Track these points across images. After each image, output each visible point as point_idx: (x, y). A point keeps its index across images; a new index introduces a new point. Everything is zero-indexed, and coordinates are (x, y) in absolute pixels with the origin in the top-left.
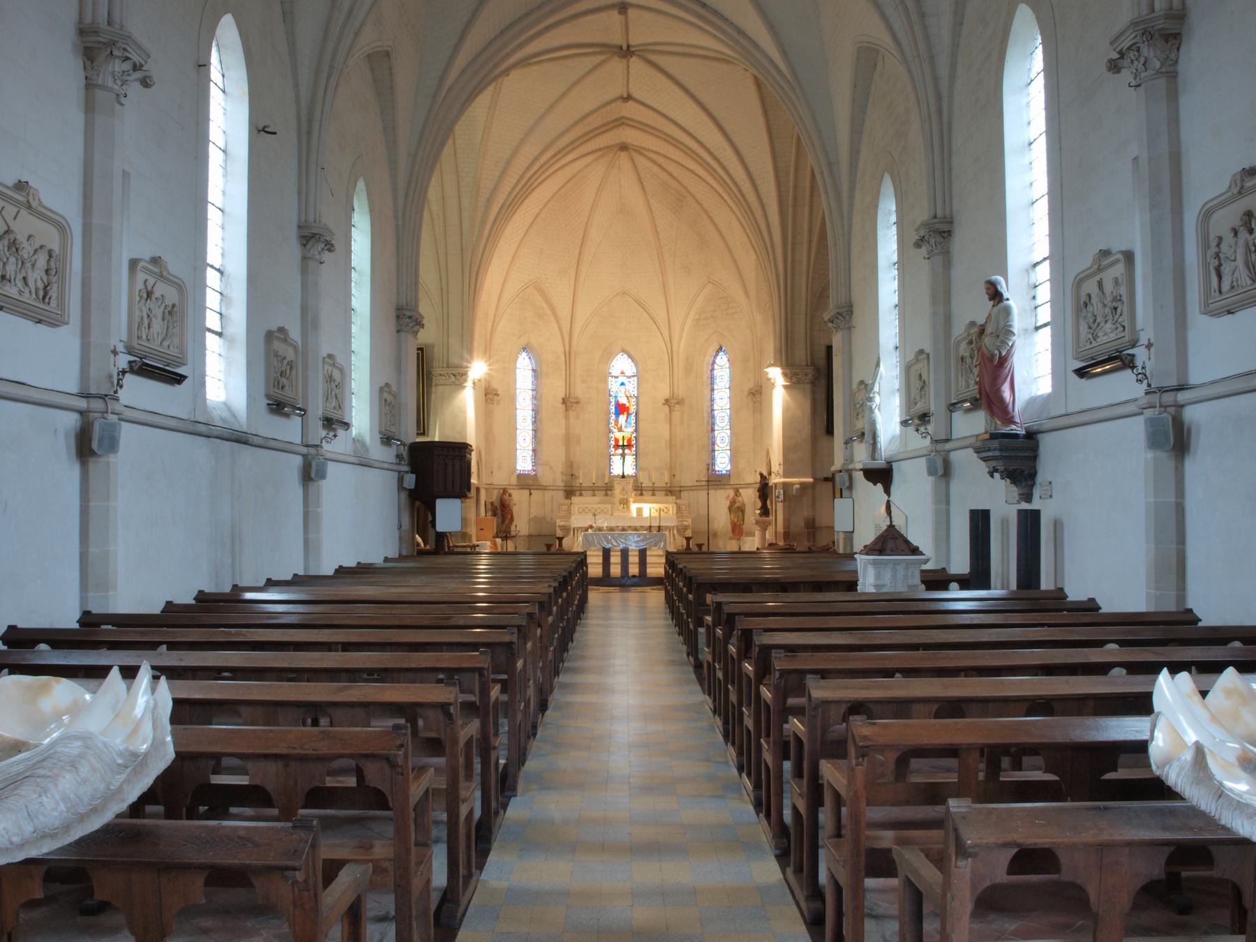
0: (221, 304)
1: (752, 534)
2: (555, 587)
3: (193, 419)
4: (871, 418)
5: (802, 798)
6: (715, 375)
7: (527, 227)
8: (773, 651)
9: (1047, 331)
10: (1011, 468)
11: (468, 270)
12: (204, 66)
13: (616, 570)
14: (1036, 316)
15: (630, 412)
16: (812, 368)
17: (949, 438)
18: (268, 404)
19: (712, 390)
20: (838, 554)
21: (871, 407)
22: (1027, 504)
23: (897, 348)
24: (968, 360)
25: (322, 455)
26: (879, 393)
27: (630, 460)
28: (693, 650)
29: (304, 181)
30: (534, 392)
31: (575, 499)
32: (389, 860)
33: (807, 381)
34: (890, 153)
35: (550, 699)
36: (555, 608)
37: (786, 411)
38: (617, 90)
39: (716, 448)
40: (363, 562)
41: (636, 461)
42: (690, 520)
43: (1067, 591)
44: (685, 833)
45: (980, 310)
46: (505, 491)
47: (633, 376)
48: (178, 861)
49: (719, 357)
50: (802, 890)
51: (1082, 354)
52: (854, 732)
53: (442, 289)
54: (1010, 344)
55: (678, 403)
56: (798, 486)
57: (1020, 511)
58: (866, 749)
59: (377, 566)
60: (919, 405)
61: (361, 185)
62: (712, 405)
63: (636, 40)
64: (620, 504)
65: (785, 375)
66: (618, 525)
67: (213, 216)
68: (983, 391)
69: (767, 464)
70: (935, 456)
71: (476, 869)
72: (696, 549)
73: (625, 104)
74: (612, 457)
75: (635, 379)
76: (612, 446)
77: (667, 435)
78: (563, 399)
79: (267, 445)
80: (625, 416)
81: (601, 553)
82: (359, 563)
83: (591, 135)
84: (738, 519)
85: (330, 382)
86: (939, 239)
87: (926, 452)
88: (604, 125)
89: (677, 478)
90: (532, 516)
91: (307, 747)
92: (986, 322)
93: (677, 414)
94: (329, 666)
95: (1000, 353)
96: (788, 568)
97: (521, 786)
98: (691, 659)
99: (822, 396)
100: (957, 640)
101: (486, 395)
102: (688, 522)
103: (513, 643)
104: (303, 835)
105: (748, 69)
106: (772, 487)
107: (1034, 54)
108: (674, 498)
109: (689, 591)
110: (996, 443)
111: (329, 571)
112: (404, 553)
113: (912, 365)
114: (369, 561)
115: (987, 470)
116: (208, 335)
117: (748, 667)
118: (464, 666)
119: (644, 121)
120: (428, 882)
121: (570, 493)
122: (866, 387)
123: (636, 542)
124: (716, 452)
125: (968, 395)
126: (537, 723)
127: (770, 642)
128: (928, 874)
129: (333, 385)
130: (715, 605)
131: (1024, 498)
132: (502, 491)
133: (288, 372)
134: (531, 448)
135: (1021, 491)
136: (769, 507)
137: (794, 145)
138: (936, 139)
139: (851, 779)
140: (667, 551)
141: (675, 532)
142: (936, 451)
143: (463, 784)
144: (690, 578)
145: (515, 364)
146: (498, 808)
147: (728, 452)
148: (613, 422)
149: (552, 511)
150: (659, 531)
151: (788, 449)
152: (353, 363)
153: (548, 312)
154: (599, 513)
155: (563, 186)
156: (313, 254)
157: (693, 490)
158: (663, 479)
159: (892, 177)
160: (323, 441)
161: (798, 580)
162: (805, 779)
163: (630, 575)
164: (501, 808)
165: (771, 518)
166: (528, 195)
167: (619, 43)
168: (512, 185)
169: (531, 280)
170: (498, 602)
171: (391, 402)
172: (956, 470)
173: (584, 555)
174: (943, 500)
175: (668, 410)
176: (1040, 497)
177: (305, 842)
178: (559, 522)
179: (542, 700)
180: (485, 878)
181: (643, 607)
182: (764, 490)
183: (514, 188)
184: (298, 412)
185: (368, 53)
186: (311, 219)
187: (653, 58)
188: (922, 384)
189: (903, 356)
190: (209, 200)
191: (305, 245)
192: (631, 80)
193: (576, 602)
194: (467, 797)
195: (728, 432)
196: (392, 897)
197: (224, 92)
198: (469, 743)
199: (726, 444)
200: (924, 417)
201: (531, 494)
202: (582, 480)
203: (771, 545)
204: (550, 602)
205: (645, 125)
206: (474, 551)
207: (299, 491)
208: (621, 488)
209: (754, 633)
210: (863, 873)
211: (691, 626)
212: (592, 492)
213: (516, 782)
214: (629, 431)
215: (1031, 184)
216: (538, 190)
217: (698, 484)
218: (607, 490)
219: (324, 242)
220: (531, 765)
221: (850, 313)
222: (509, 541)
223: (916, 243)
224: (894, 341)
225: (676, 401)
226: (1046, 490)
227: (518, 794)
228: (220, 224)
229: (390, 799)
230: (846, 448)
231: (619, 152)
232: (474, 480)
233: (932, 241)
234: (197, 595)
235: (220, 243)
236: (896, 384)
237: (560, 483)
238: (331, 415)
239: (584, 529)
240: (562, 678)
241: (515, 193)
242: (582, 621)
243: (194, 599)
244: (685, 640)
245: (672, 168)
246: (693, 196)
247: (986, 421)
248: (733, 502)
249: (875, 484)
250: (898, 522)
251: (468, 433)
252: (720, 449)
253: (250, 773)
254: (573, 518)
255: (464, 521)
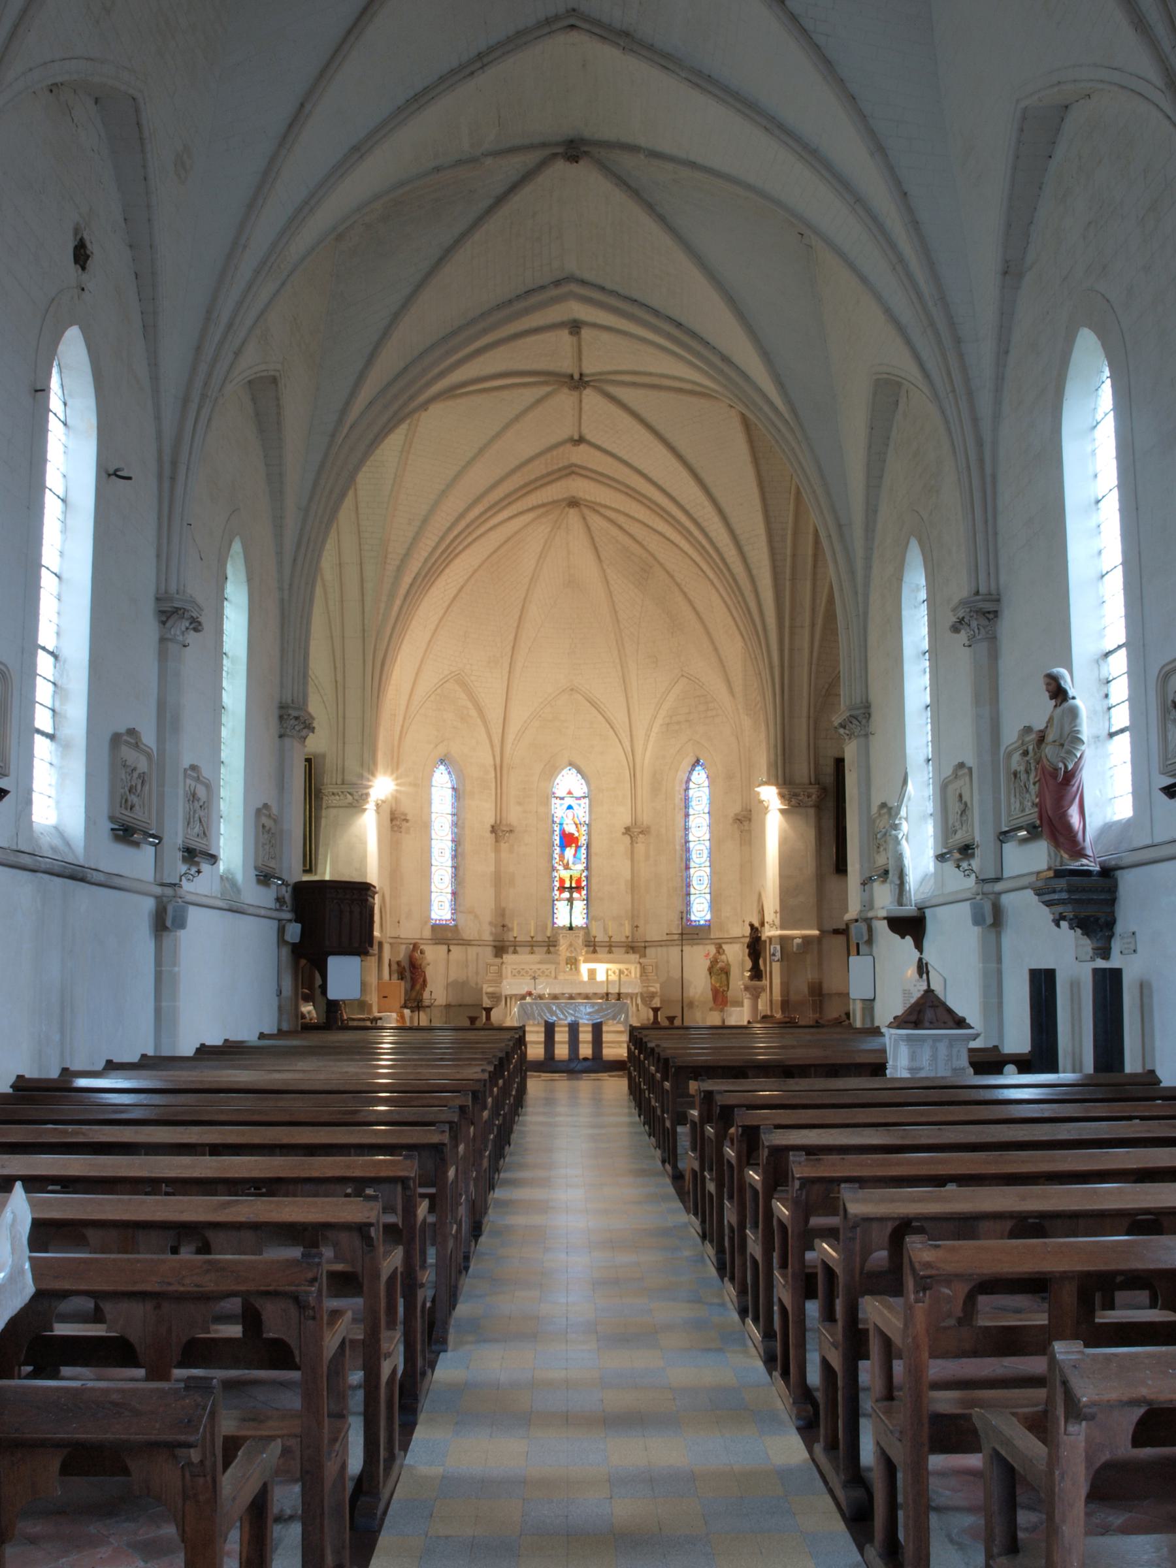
0: (53, 697)
1: (740, 1004)
2: (490, 1072)
3: (14, 847)
4: (897, 851)
5: (836, 1348)
6: (690, 796)
7: (446, 604)
8: (791, 1153)
9: (1125, 740)
10: (1082, 915)
11: (371, 657)
12: (41, 391)
13: (562, 1051)
14: (1109, 719)
15: (579, 844)
16: (817, 786)
17: (1000, 876)
18: (112, 829)
19: (687, 815)
20: (856, 1029)
21: (897, 837)
22: (1104, 961)
23: (929, 760)
24: (1023, 776)
25: (180, 898)
26: (906, 819)
27: (579, 906)
28: (670, 1155)
29: (165, 541)
30: (455, 818)
31: (508, 958)
32: (296, 1436)
33: (811, 803)
34: (917, 512)
35: (485, 1220)
36: (490, 1100)
37: (783, 842)
38: (567, 430)
39: (692, 891)
40: (232, 1039)
41: (587, 908)
42: (658, 986)
43: (1160, 1073)
44: (674, 1399)
45: (1039, 711)
46: (415, 946)
47: (584, 797)
48: (29, 1436)
49: (695, 773)
50: (838, 1474)
51: (1171, 768)
52: (913, 1257)
53: (336, 682)
54: (1078, 756)
55: (642, 832)
56: (799, 941)
57: (1096, 971)
58: (928, 1280)
59: (251, 1044)
60: (959, 835)
61: (237, 547)
62: (687, 835)
63: (589, 368)
64: (567, 964)
65: (782, 796)
66: (564, 992)
67: (48, 582)
68: (1044, 815)
69: (759, 912)
70: (981, 899)
71: (400, 1450)
72: (666, 1023)
73: (575, 448)
74: (556, 902)
75: (587, 800)
76: (556, 888)
77: (627, 874)
78: (493, 827)
79: (110, 883)
80: (573, 849)
81: (543, 1029)
82: (226, 1041)
83: (533, 486)
84: (721, 983)
85: (193, 802)
86: (984, 622)
87: (968, 895)
88: (549, 474)
89: (641, 930)
90: (450, 980)
91: (187, 1281)
92: (1047, 727)
93: (640, 848)
94: (203, 1176)
95: (1066, 767)
96: (793, 1047)
97: (451, 1338)
98: (668, 1167)
99: (829, 824)
100: (1026, 1138)
101: (392, 820)
102: (656, 988)
103: (444, 1145)
104: (200, 1399)
105: (734, 405)
106: (765, 941)
107: (1100, 390)
108: (637, 956)
109: (665, 1077)
110: (1062, 883)
111: (189, 1050)
112: (285, 1027)
113: (950, 782)
114: (239, 1038)
115: (1051, 917)
116: (37, 737)
117: (754, 1176)
118: (383, 1174)
119: (600, 469)
120: (344, 1466)
121: (500, 949)
122: (890, 811)
123: (589, 1014)
124: (692, 896)
125: (1023, 821)
126: (469, 1252)
127: (784, 1142)
128: (1029, 1446)
129: (197, 805)
130: (702, 1094)
131: (1101, 954)
132: (411, 946)
133: (139, 787)
134: (449, 890)
135: (1096, 945)
136: (762, 967)
137: (792, 501)
138: (977, 495)
139: (908, 1320)
140: (631, 1026)
141: (639, 1001)
142: (983, 894)
143: (384, 1334)
144: (667, 1060)
145: (431, 781)
146: (424, 1366)
147: (708, 896)
148: (556, 856)
149: (477, 973)
150: (619, 999)
151: (787, 892)
152: (222, 776)
153: (473, 713)
154: (539, 976)
155: (495, 552)
156: (175, 635)
157: (661, 946)
158: (622, 932)
159: (920, 542)
160: (183, 878)
161: (808, 1062)
162: (840, 1324)
163: (581, 1057)
164: (429, 1367)
165: (765, 982)
166: (450, 562)
167: (569, 371)
168: (430, 549)
169: (454, 672)
170: (405, 1093)
171: (270, 829)
172: (1010, 919)
173: (522, 1030)
174: (993, 956)
175: (630, 842)
176: (1121, 952)
177: (203, 1409)
178: (487, 988)
179: (474, 1222)
180: (412, 1463)
181: (597, 1100)
182: (755, 946)
183: (431, 554)
184: (151, 840)
185: (249, 379)
186: (173, 588)
187: (612, 390)
188: (962, 807)
189: (937, 770)
190: (44, 563)
191: (164, 623)
192: (584, 417)
193: (514, 1093)
194: (390, 1350)
195: (708, 870)
196: (297, 1488)
197: (65, 424)
198: (392, 1278)
199: (705, 886)
200: (966, 850)
201: (449, 951)
202: (517, 932)
203: (765, 1017)
204: (485, 1092)
205: (602, 474)
206: (374, 1025)
207: (150, 945)
208: (568, 943)
209: (761, 1131)
210: (926, 1449)
211: (668, 1124)
212: (529, 948)
213: (446, 1331)
214: (578, 868)
215: (1100, 552)
216: (463, 556)
217: (669, 938)
218: (549, 946)
219: (187, 619)
220: (463, 1309)
221: (867, 716)
222: (421, 1013)
223: (953, 626)
224: (925, 751)
225: (640, 830)
226: (1128, 943)
227: (450, 1348)
228: (55, 593)
229: (296, 1352)
230: (864, 891)
231: (567, 509)
232: (376, 933)
233: (974, 624)
234: (14, 1083)
235: (55, 619)
236: (929, 807)
237: (487, 937)
238: (193, 845)
239: (518, 997)
240: (498, 1194)
241: (433, 560)
242: (520, 1118)
243: (11, 1087)
244: (658, 1141)
245: (635, 529)
246: (661, 564)
247: (1049, 855)
248: (714, 962)
249: (903, 937)
250: (936, 986)
251: (368, 871)
252: (697, 892)
253: (108, 1317)
254: (505, 982)
255: (364, 986)
